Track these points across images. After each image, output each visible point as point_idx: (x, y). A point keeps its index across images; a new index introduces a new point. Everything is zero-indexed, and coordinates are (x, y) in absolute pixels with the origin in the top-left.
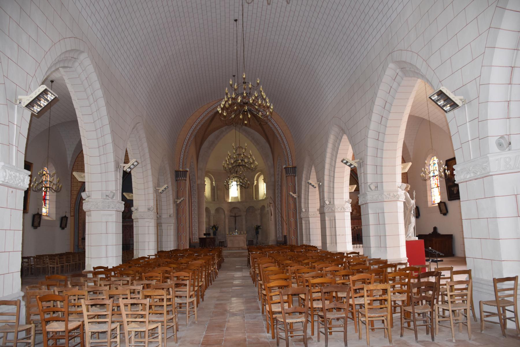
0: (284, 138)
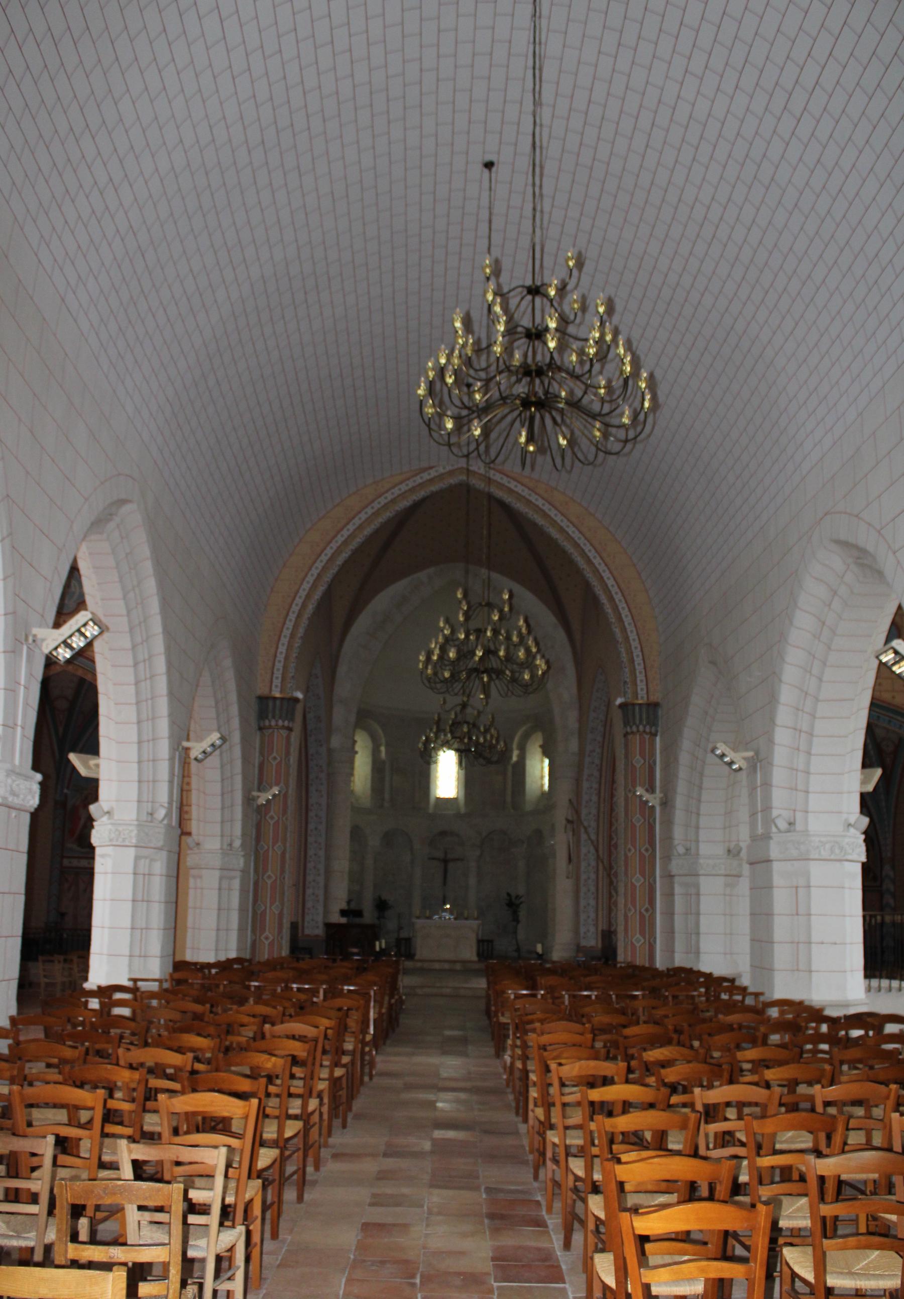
0: (622, 605)
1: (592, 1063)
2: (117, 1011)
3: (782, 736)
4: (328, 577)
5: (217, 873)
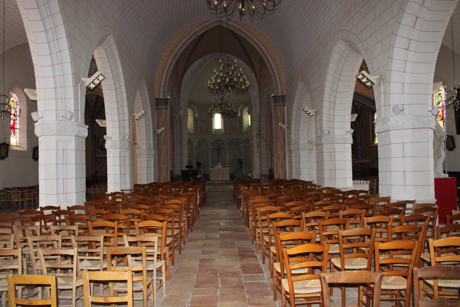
0: (272, 64)
1: (270, 207)
2: (117, 200)
3: (326, 104)
4: (176, 58)
5: (146, 156)
